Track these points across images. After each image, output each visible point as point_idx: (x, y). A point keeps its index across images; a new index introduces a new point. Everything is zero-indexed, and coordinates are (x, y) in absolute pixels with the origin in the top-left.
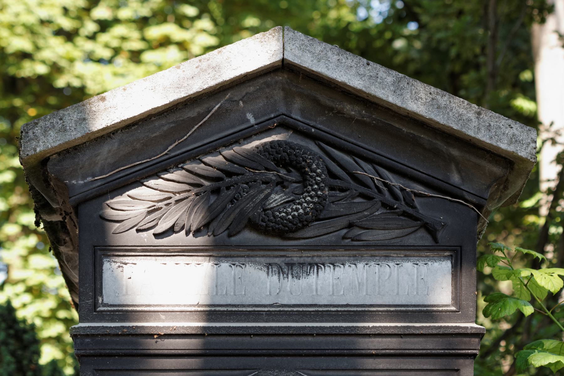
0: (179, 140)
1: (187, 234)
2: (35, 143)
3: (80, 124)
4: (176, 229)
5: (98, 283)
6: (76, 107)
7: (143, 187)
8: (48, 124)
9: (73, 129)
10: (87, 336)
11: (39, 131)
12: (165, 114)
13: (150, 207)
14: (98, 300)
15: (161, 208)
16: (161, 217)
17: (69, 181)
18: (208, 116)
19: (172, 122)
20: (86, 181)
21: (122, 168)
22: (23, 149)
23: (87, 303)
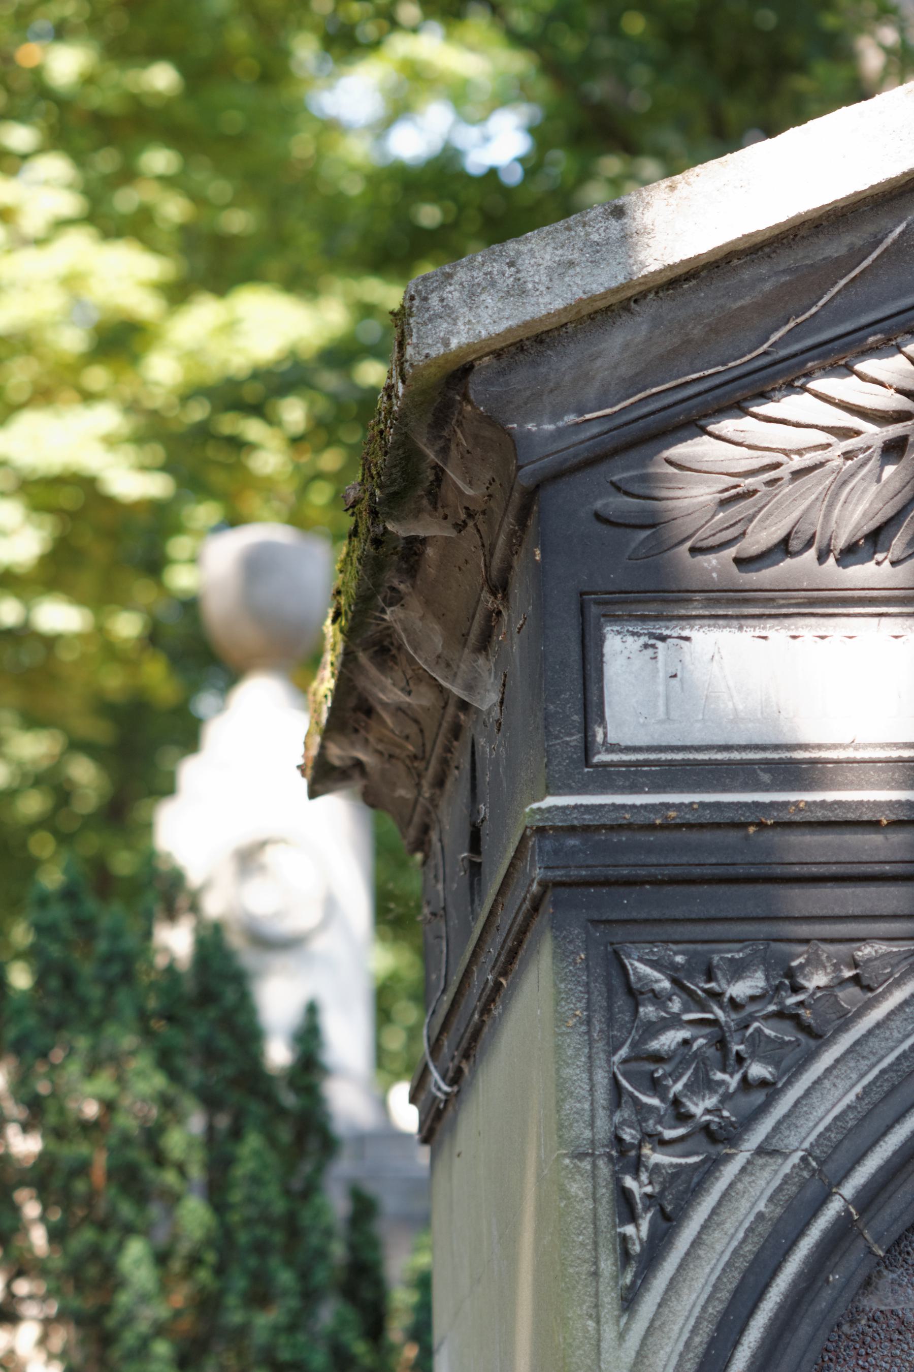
0: (797, 317)
1: (822, 557)
2: (445, 325)
3: (562, 275)
4: (795, 545)
5: (593, 689)
6: (549, 233)
7: (706, 438)
8: (479, 276)
9: (542, 288)
10: (572, 830)
11: (456, 294)
12: (767, 250)
13: (726, 490)
14: (594, 736)
15: (755, 492)
16: (754, 516)
17: (520, 426)
18: (874, 255)
19: (784, 271)
20: (560, 424)
21: (654, 390)
22: (414, 340)
23: (567, 743)
